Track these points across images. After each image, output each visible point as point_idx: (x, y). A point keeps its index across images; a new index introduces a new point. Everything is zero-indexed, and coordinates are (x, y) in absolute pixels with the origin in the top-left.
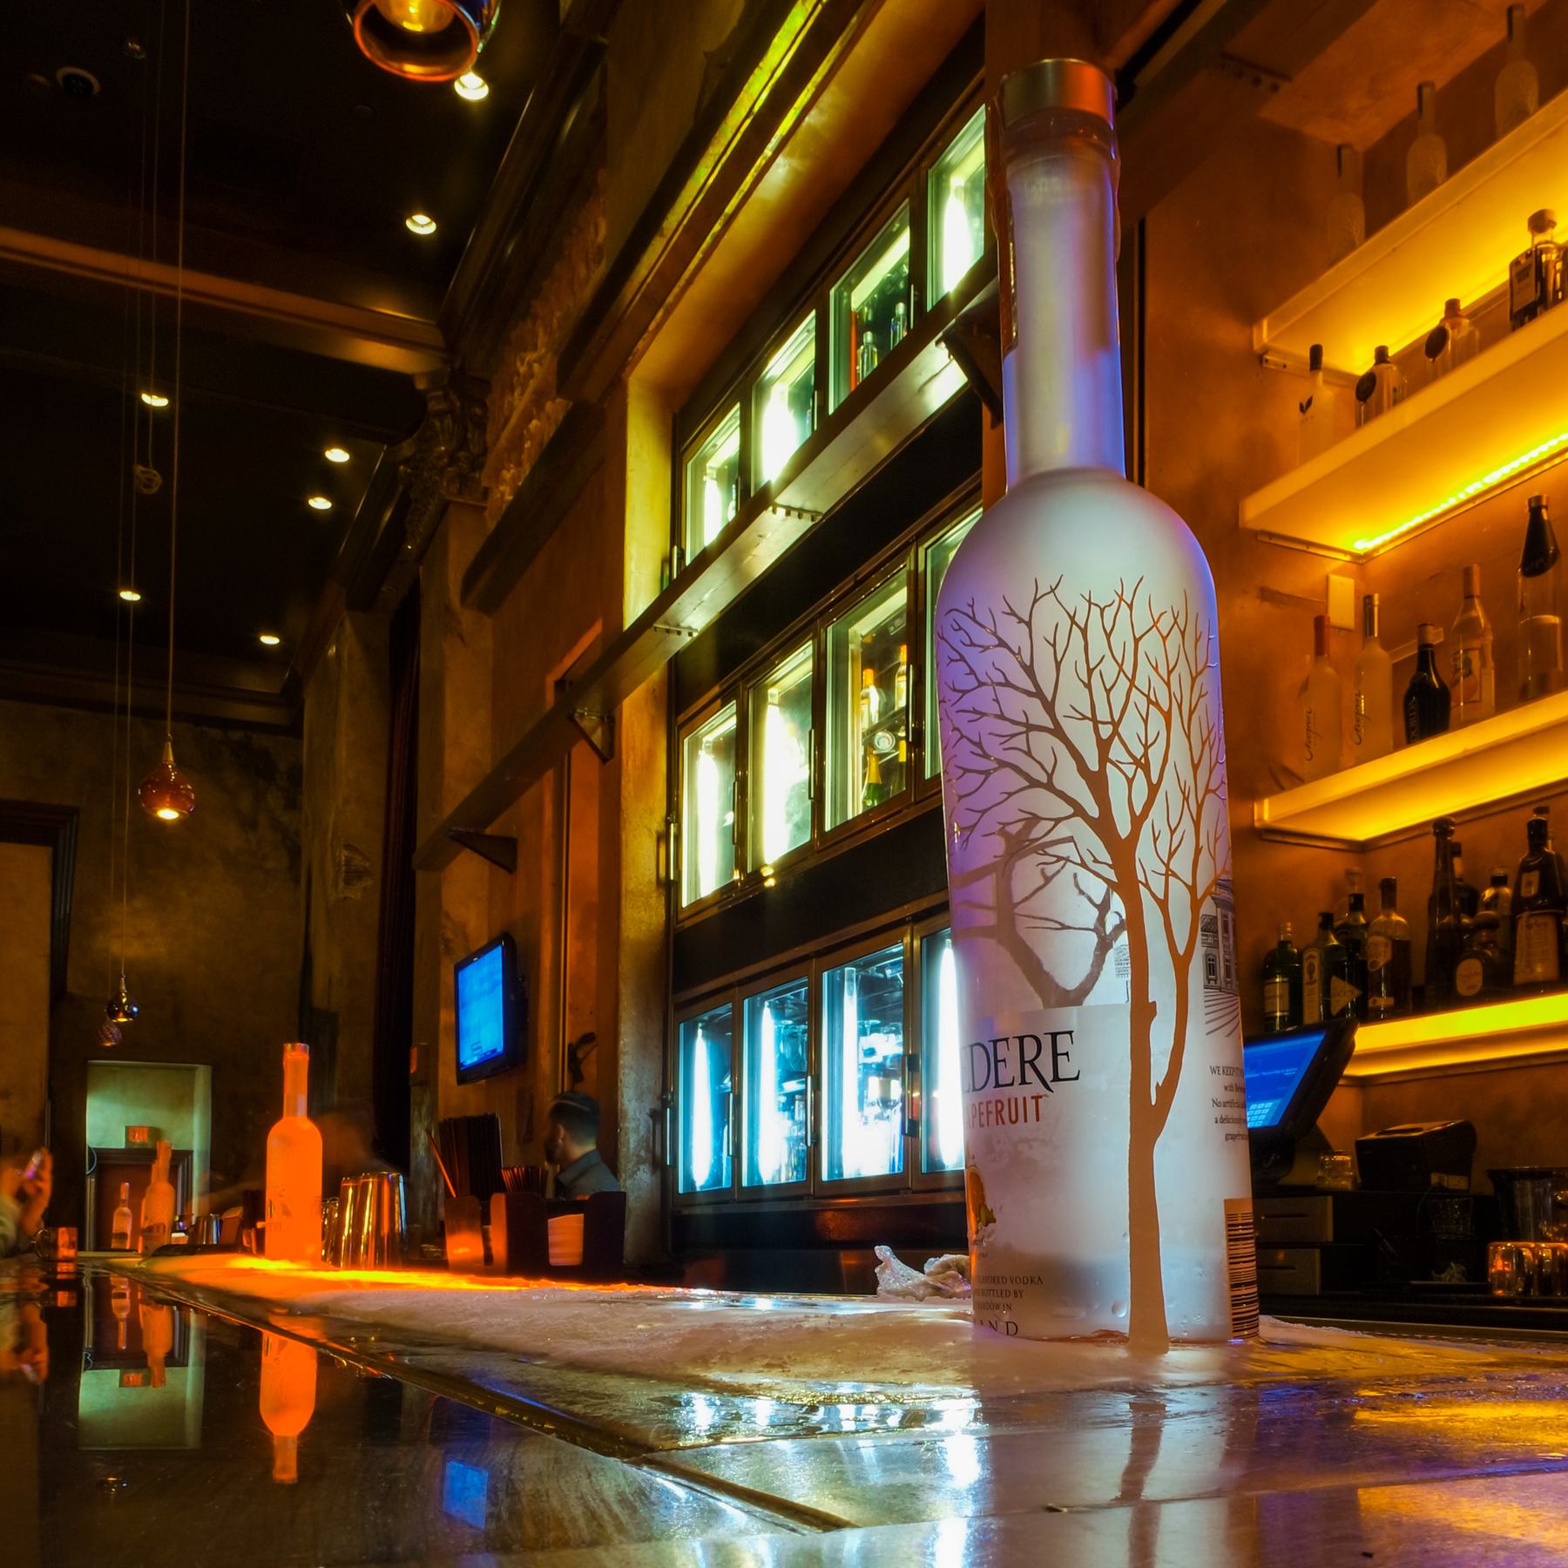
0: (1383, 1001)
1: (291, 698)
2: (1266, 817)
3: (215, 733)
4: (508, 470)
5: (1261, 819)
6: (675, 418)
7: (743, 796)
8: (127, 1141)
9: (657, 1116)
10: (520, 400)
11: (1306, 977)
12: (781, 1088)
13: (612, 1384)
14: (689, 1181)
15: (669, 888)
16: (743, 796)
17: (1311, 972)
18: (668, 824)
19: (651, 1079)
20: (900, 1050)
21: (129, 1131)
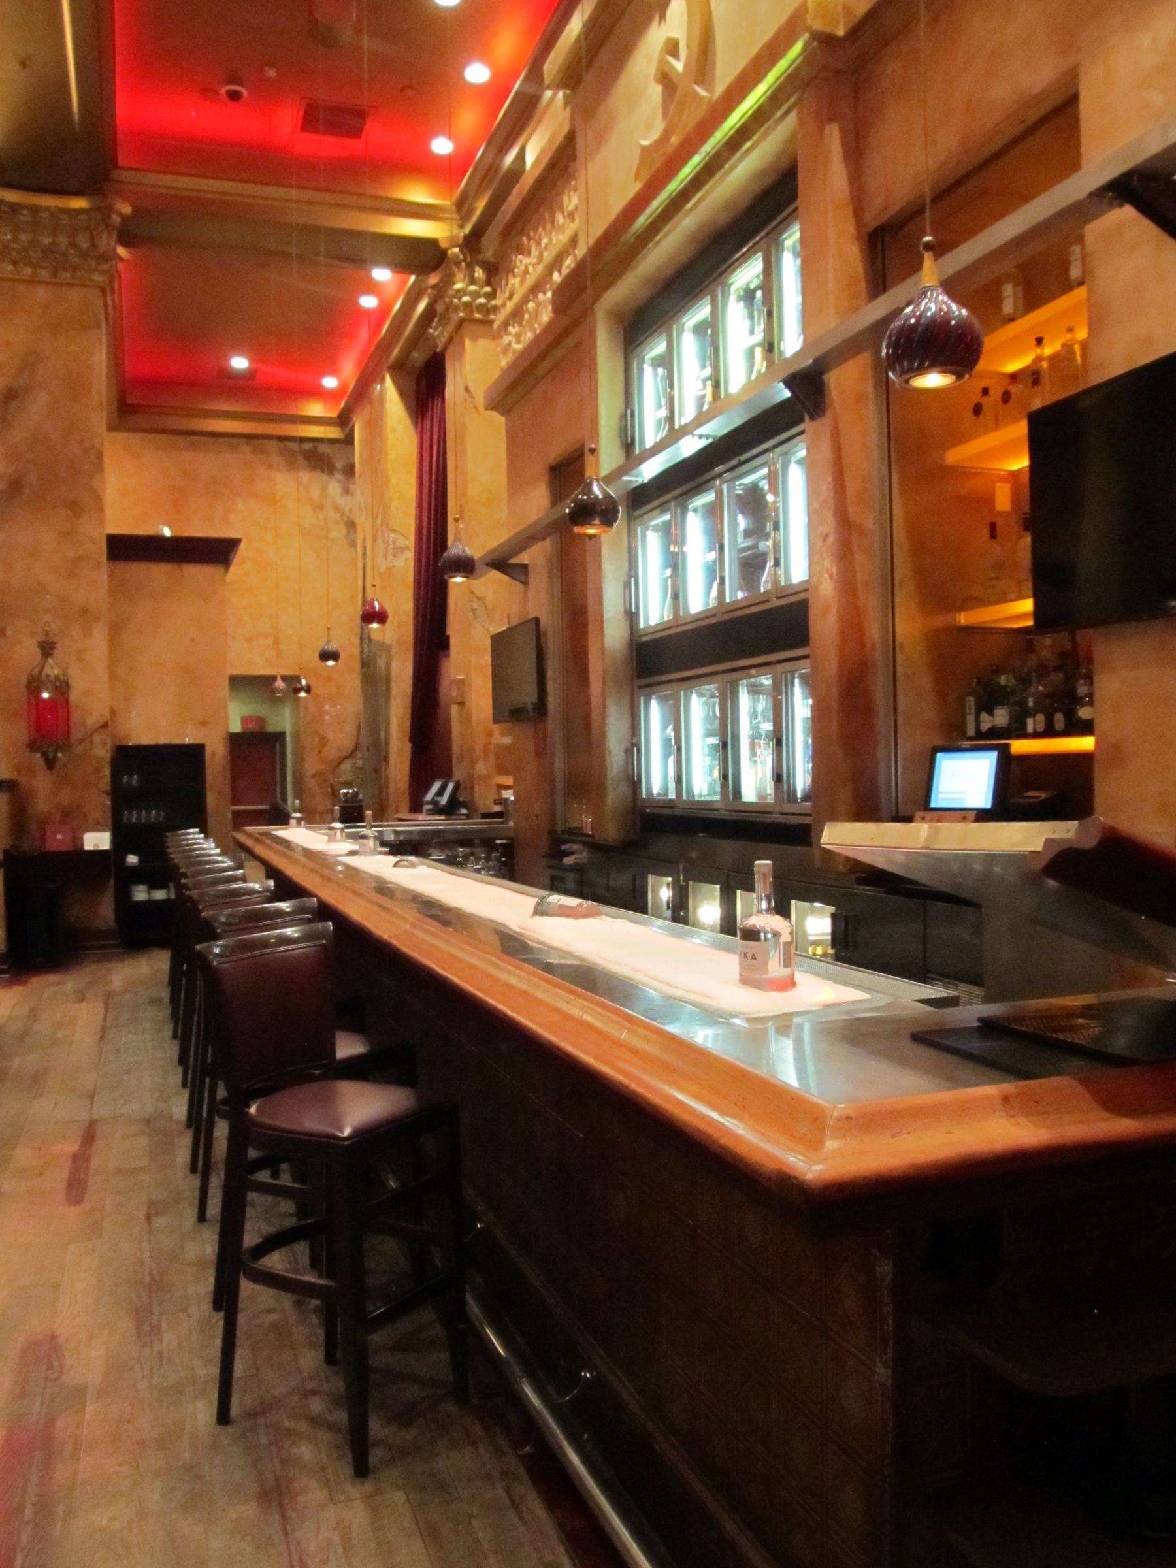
0: (571, 885)
1: (344, 420)
2: (962, 621)
3: (293, 446)
4: (514, 327)
5: (960, 622)
6: (625, 329)
7: (675, 563)
8: (243, 727)
9: (628, 751)
10: (521, 286)
11: (968, 711)
12: (704, 741)
13: (430, 413)
14: (649, 788)
15: (632, 617)
16: (675, 563)
17: (970, 708)
18: (630, 577)
19: (626, 723)
20: (771, 728)
21: (245, 720)
